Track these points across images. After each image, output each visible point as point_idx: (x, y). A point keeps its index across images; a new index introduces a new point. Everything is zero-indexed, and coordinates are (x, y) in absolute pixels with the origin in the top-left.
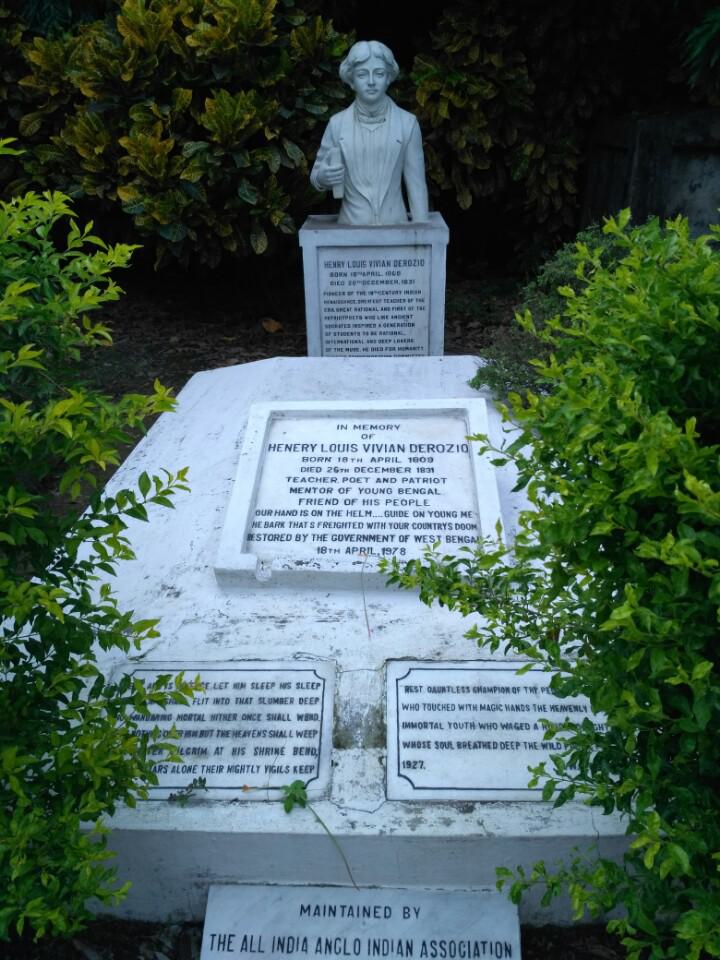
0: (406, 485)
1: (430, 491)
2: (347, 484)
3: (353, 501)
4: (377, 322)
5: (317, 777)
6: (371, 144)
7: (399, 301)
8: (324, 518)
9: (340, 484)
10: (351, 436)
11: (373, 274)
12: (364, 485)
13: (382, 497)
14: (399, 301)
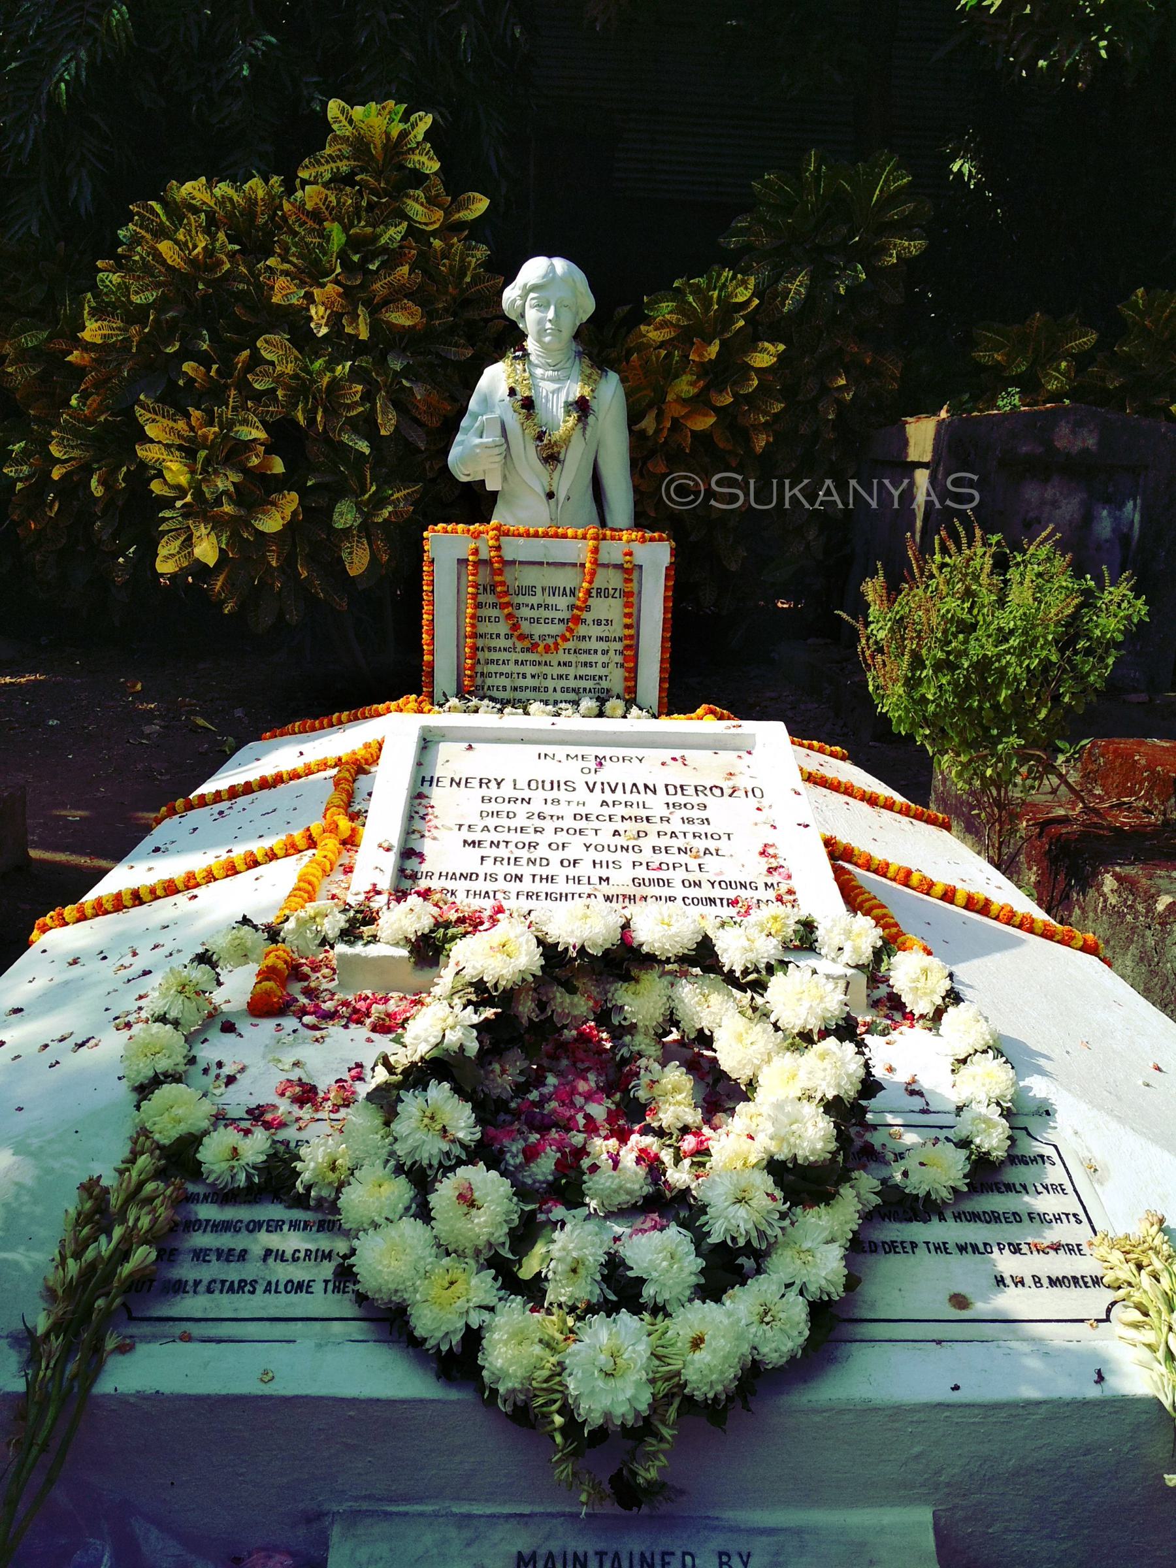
0: (664, 841)
1: (707, 851)
2: (561, 838)
3: (575, 862)
4: (550, 684)
5: (1055, 1146)
6: (536, 389)
7: (588, 652)
8: (527, 885)
9: (548, 836)
10: (570, 771)
11: (547, 607)
12: (591, 838)
13: (626, 858)
14: (588, 652)
